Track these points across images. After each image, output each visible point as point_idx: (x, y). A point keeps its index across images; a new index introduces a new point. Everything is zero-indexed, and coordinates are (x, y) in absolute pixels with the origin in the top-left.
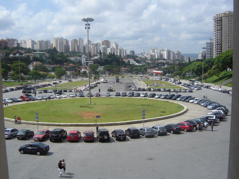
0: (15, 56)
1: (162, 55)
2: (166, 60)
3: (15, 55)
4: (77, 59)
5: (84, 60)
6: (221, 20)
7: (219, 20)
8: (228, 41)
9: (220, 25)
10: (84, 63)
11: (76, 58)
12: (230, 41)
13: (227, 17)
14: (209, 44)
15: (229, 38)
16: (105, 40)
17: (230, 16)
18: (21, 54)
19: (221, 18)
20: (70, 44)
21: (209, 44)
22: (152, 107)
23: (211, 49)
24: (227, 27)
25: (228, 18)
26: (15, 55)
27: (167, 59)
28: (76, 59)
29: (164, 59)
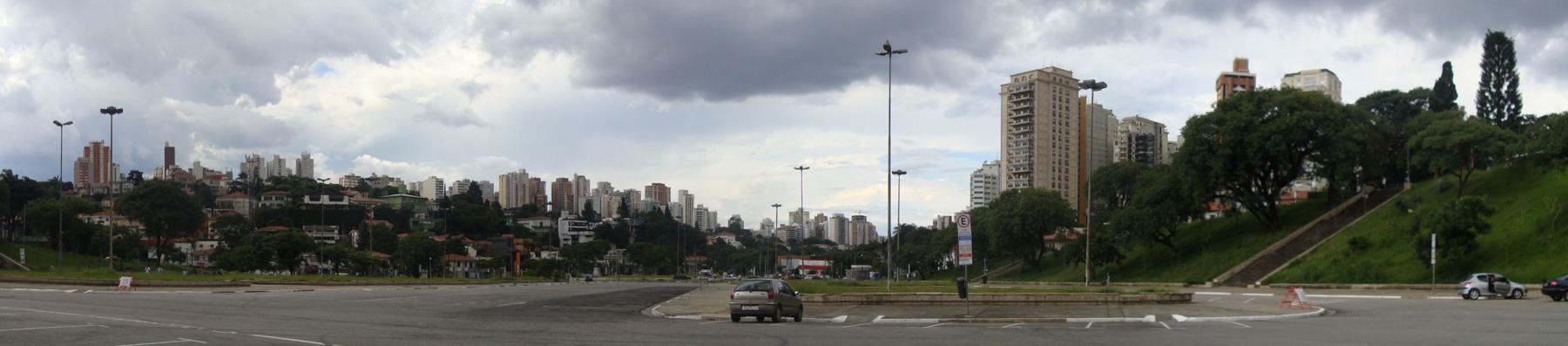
0: (317, 203)
1: (823, 229)
2: (834, 244)
3: (319, 200)
4: (544, 225)
5: (567, 227)
6: (1031, 93)
7: (1025, 94)
8: (1051, 165)
9: (1026, 116)
10: (566, 237)
11: (541, 223)
12: (1057, 165)
13: (1048, 83)
14: (982, 179)
15: (1054, 155)
16: (653, 184)
17: (1058, 81)
18: (336, 197)
19: (1031, 84)
20: (548, 192)
21: (982, 179)
22: (1164, 291)
23: (987, 196)
24: (1047, 124)
25: (1052, 89)
26: (319, 200)
27: (838, 242)
28: (539, 225)
29: (828, 242)
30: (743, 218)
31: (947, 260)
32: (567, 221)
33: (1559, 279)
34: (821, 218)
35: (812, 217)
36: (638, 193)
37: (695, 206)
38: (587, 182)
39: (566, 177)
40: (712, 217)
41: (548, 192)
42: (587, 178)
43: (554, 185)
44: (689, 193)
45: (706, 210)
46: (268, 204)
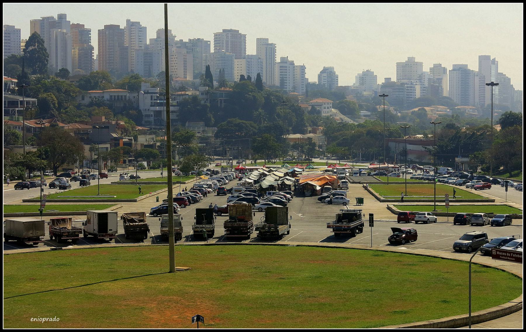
5: (148, 101)
16: (224, 31)
20: (94, 42)
30: (337, 71)
31: (213, 139)
32: (149, 95)
33: (423, 149)
34: (438, 69)
35: (426, 69)
36: (207, 44)
37: (278, 60)
38: (143, 30)
39: (487, 54)
40: (298, 72)
41: (94, 42)
42: (143, 25)
43: (101, 33)
44: (270, 42)
45: (292, 63)
46: (223, 88)
